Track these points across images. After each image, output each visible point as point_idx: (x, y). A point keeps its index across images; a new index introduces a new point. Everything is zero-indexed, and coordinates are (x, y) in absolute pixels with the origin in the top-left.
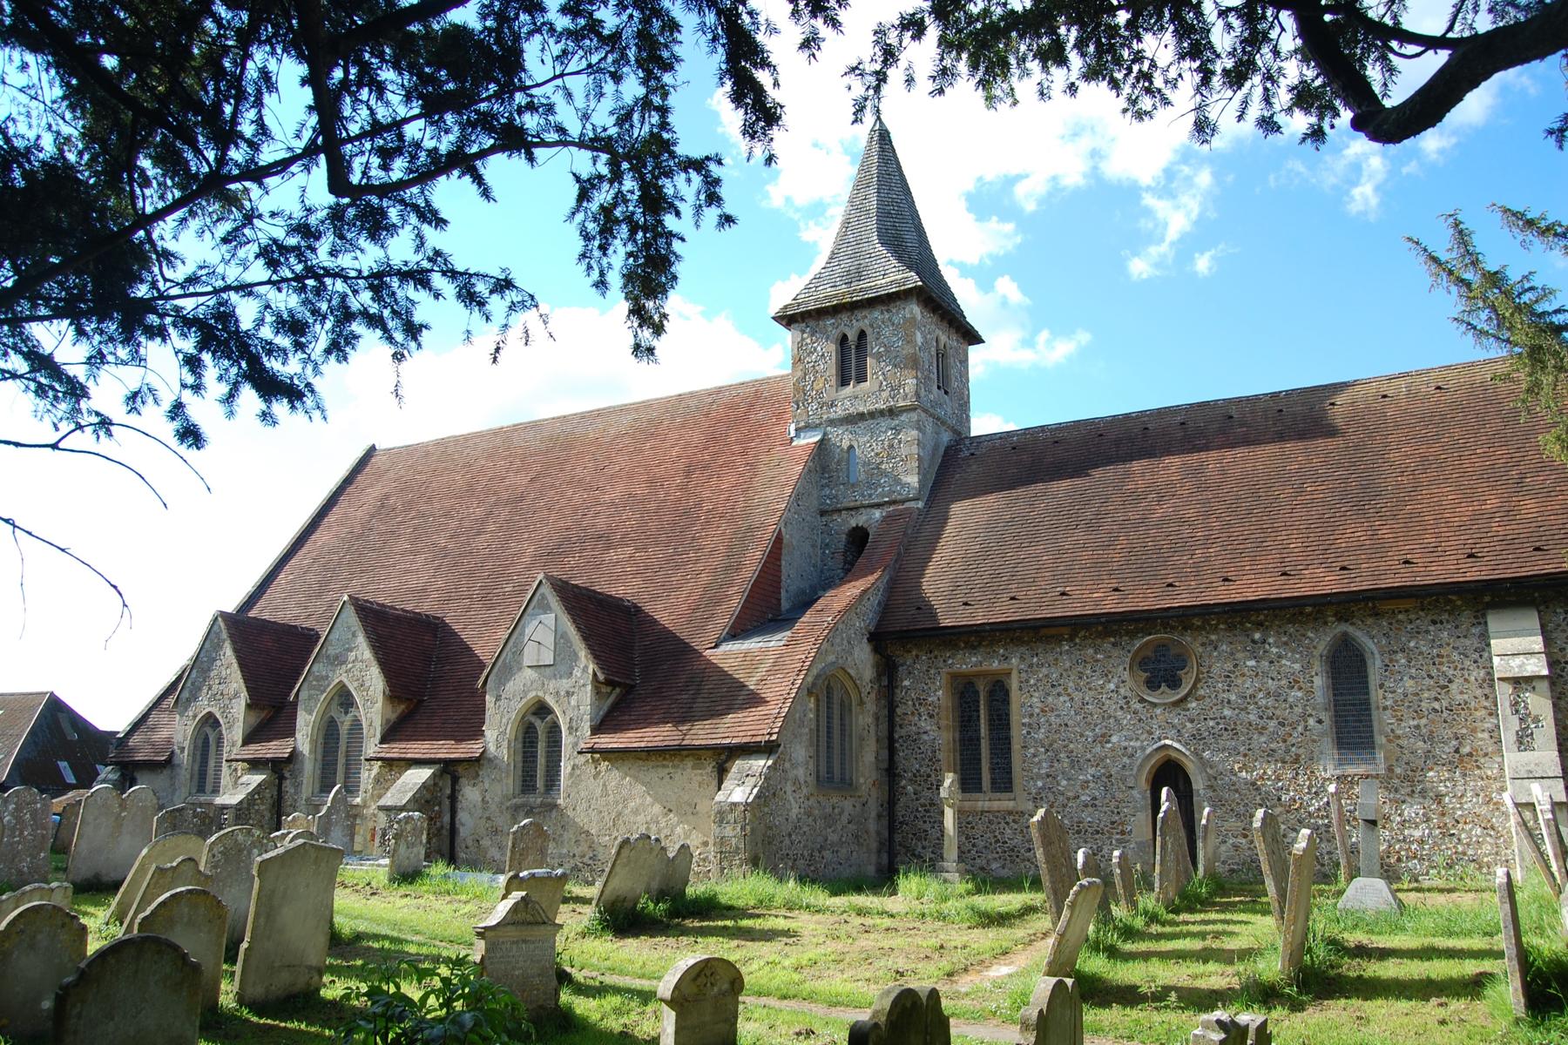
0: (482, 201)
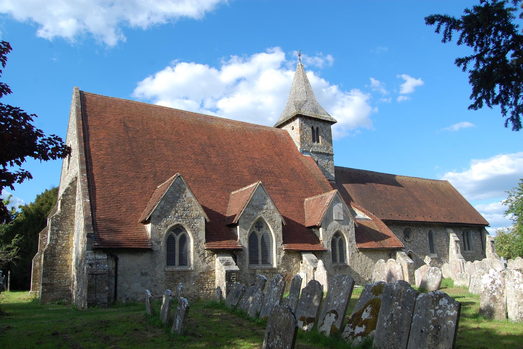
0: (504, 126)
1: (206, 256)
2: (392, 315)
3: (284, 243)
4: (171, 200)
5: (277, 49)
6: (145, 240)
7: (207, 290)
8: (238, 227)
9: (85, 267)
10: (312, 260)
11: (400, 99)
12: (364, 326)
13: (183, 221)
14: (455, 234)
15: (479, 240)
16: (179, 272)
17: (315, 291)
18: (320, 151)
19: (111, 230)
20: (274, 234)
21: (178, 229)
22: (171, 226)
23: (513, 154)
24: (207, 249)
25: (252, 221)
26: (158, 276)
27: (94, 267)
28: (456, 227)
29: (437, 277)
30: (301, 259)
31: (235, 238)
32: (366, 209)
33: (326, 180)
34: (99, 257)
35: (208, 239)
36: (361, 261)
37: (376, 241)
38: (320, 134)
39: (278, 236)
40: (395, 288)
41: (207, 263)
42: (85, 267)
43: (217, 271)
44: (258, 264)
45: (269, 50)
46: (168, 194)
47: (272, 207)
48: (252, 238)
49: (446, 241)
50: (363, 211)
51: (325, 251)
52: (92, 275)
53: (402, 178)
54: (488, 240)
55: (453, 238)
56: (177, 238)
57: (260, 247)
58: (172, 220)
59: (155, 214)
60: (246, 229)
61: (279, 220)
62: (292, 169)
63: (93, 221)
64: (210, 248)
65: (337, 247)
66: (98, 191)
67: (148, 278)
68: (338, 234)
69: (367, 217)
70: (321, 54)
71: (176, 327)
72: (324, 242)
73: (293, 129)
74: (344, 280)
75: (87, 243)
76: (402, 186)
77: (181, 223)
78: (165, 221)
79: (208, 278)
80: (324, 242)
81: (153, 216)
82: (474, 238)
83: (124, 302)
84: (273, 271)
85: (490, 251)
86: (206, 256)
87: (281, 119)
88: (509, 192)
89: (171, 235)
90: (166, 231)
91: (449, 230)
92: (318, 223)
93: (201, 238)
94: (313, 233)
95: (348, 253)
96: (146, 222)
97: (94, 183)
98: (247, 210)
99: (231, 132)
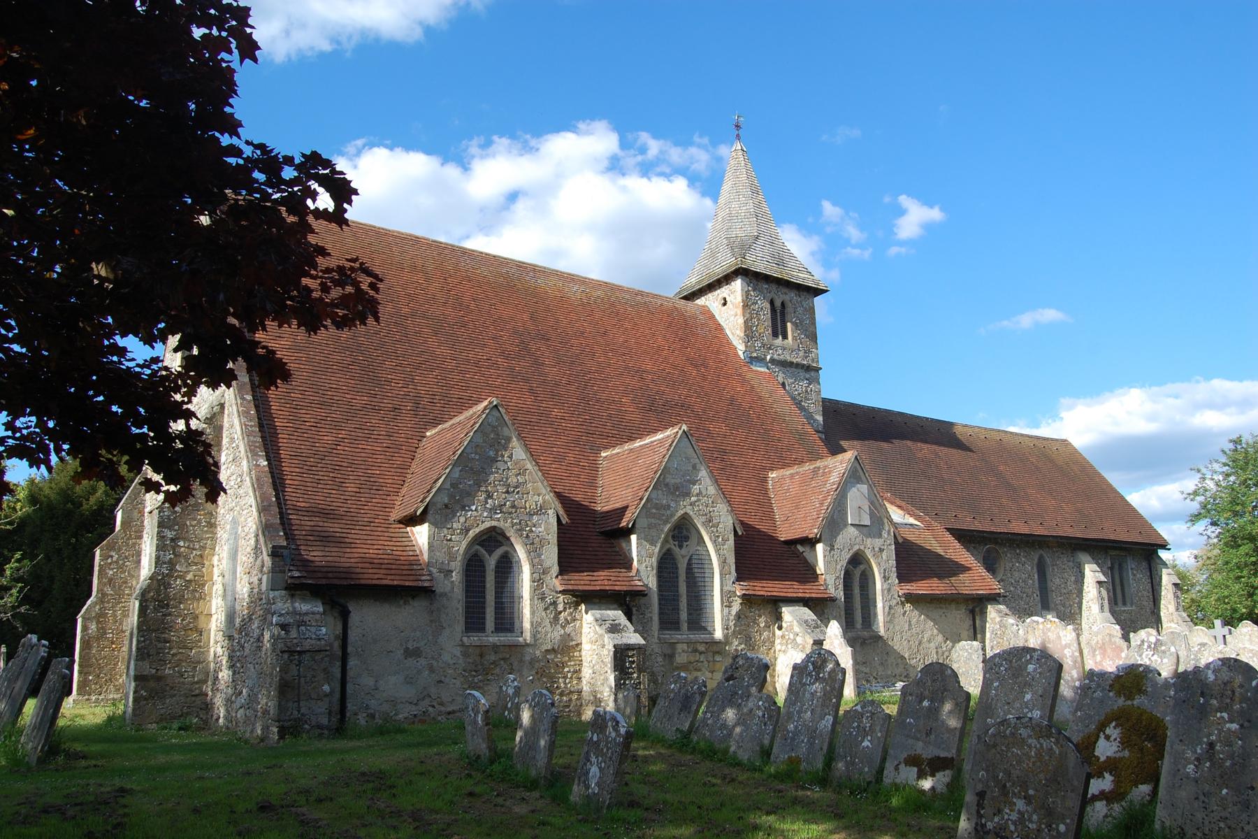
1: (560, 607)
2: (1211, 745)
3: (739, 579)
4: (476, 465)
5: (601, 126)
6: (412, 564)
7: (562, 694)
8: (634, 538)
9: (267, 636)
10: (806, 622)
11: (894, 250)
12: (1107, 775)
13: (505, 520)
14: (1095, 567)
15: (1146, 581)
16: (495, 648)
17: (945, 690)
18: (789, 359)
19: (325, 539)
20: (717, 555)
21: (493, 539)
22: (478, 530)
23: (1155, 389)
24: (564, 592)
25: (666, 522)
26: (446, 657)
27: (294, 634)
28: (1100, 549)
29: (1165, 660)
30: (779, 618)
31: (628, 564)
32: (911, 502)
33: (809, 429)
34: (304, 607)
35: (566, 566)
36: (910, 625)
37: (940, 577)
38: (788, 317)
39: (724, 562)
40: (1211, 677)
41: (563, 627)
42: (267, 636)
43: (586, 647)
44: (678, 629)
45: (582, 126)
46: (469, 450)
47: (712, 490)
48: (666, 565)
49: (1076, 582)
50: (899, 507)
51: (833, 600)
52: (290, 653)
53: (970, 431)
54: (1167, 579)
55: (1092, 574)
56: (491, 562)
57: (683, 589)
58: (478, 518)
59: (438, 499)
60: (653, 543)
61: (726, 521)
62: (732, 400)
63: (282, 515)
64: (570, 587)
65: (857, 591)
66: (283, 440)
67: (423, 661)
68: (857, 560)
69: (912, 521)
70: (706, 140)
71: (587, 787)
72: (828, 577)
73: (725, 304)
74: (1029, 662)
75: (273, 570)
76: (971, 451)
77: (501, 524)
78: (462, 519)
79: (564, 665)
80: (828, 577)
81: (435, 504)
82: (1135, 577)
83: (363, 722)
84: (715, 648)
85: (1172, 608)
86: (560, 607)
87: (692, 280)
88: (1199, 471)
89: (476, 555)
90: (464, 545)
91: (1083, 557)
92: (814, 532)
93: (547, 564)
94: (799, 556)
95: (880, 604)
96: (413, 520)
97: (271, 418)
98: (653, 496)
99: (583, 305)
